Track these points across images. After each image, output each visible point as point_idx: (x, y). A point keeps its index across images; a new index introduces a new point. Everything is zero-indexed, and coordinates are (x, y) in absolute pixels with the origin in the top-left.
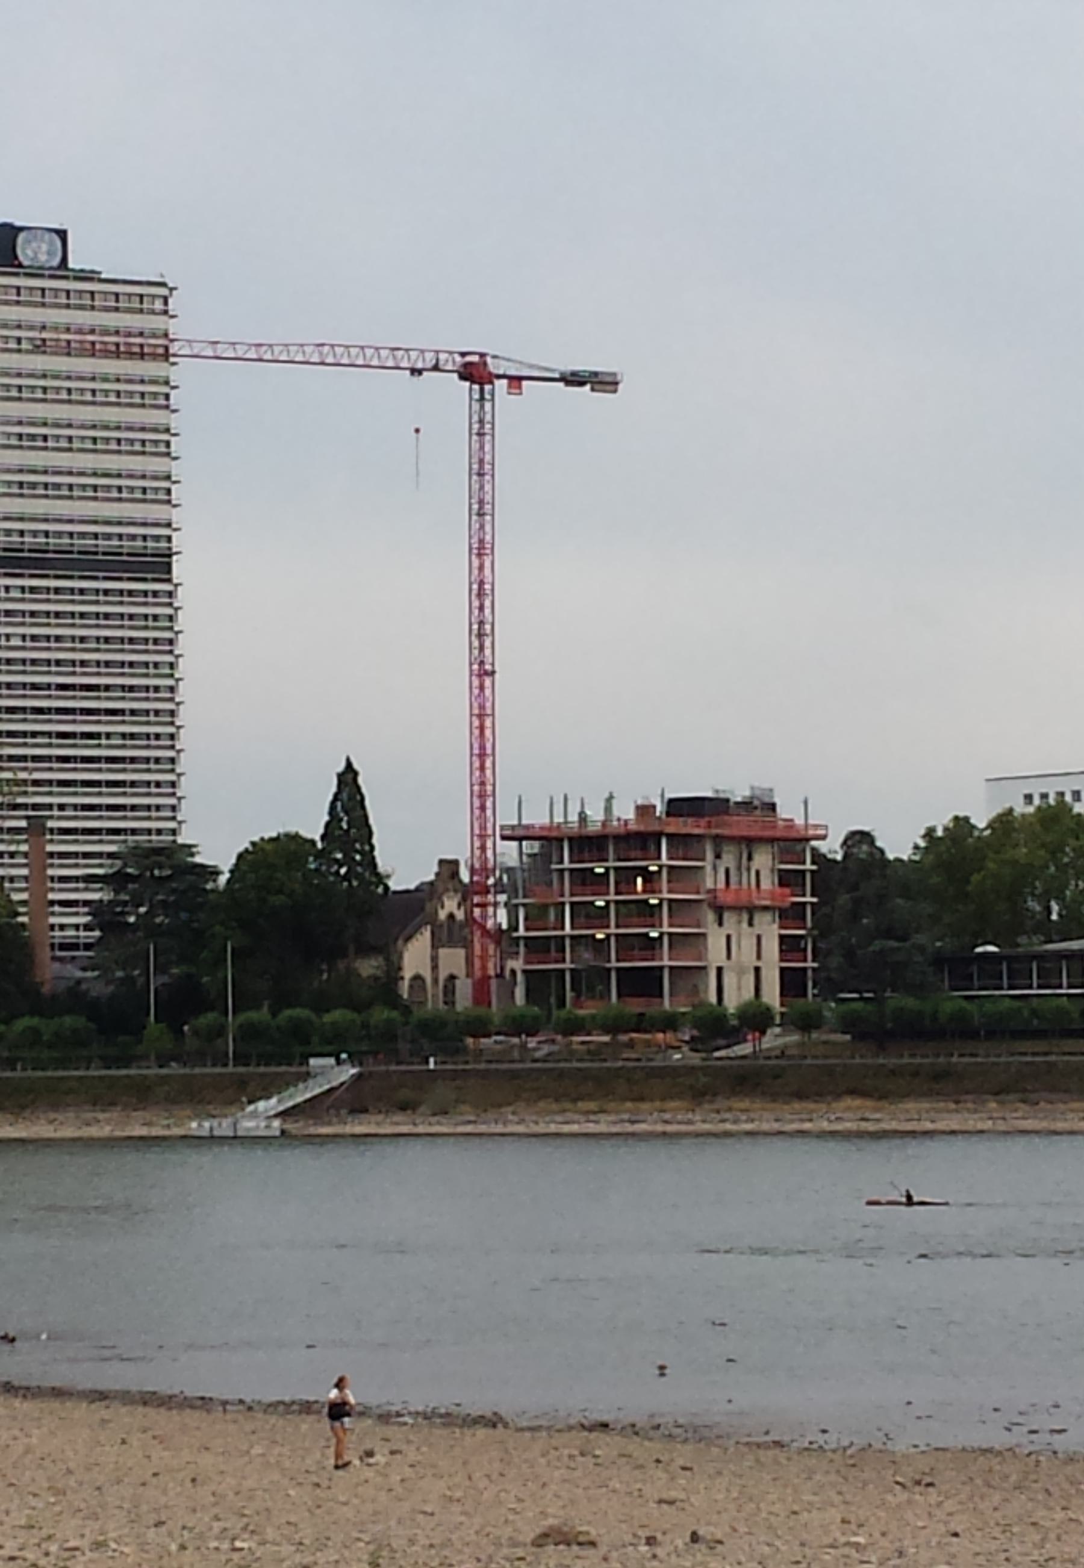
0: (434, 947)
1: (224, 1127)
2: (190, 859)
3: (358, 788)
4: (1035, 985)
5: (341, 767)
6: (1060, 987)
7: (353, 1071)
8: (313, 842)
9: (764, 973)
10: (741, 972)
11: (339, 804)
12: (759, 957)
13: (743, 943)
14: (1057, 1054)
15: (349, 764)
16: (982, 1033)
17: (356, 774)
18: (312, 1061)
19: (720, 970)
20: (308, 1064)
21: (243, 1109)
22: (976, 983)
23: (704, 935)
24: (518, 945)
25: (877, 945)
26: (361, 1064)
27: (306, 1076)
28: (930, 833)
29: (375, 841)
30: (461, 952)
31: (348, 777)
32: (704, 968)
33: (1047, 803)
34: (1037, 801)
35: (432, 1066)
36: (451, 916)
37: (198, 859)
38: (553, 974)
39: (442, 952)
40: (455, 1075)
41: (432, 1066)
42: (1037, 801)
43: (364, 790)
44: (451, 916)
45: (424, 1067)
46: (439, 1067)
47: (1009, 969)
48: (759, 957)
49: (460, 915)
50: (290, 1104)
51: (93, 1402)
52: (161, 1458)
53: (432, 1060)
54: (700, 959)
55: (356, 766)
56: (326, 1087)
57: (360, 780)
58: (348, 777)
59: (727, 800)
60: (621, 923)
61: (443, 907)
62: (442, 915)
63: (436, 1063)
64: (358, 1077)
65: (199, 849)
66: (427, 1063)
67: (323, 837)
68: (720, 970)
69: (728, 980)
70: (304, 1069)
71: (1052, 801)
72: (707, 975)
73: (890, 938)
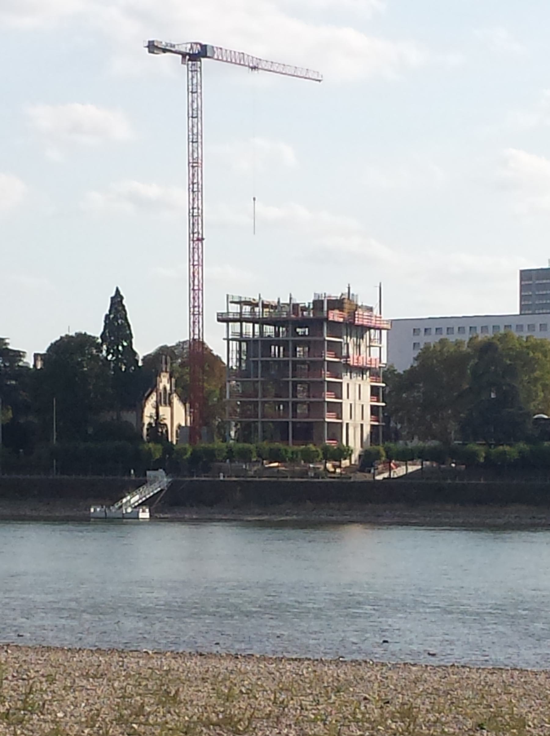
5: (113, 294)
15: (117, 291)
17: (122, 298)
18: (148, 473)
19: (347, 424)
20: (146, 475)
26: (173, 477)
30: (168, 409)
34: (491, 329)
37: (10, 347)
43: (127, 308)
44: (165, 388)
46: (226, 479)
57: (124, 302)
65: (7, 341)
68: (347, 424)
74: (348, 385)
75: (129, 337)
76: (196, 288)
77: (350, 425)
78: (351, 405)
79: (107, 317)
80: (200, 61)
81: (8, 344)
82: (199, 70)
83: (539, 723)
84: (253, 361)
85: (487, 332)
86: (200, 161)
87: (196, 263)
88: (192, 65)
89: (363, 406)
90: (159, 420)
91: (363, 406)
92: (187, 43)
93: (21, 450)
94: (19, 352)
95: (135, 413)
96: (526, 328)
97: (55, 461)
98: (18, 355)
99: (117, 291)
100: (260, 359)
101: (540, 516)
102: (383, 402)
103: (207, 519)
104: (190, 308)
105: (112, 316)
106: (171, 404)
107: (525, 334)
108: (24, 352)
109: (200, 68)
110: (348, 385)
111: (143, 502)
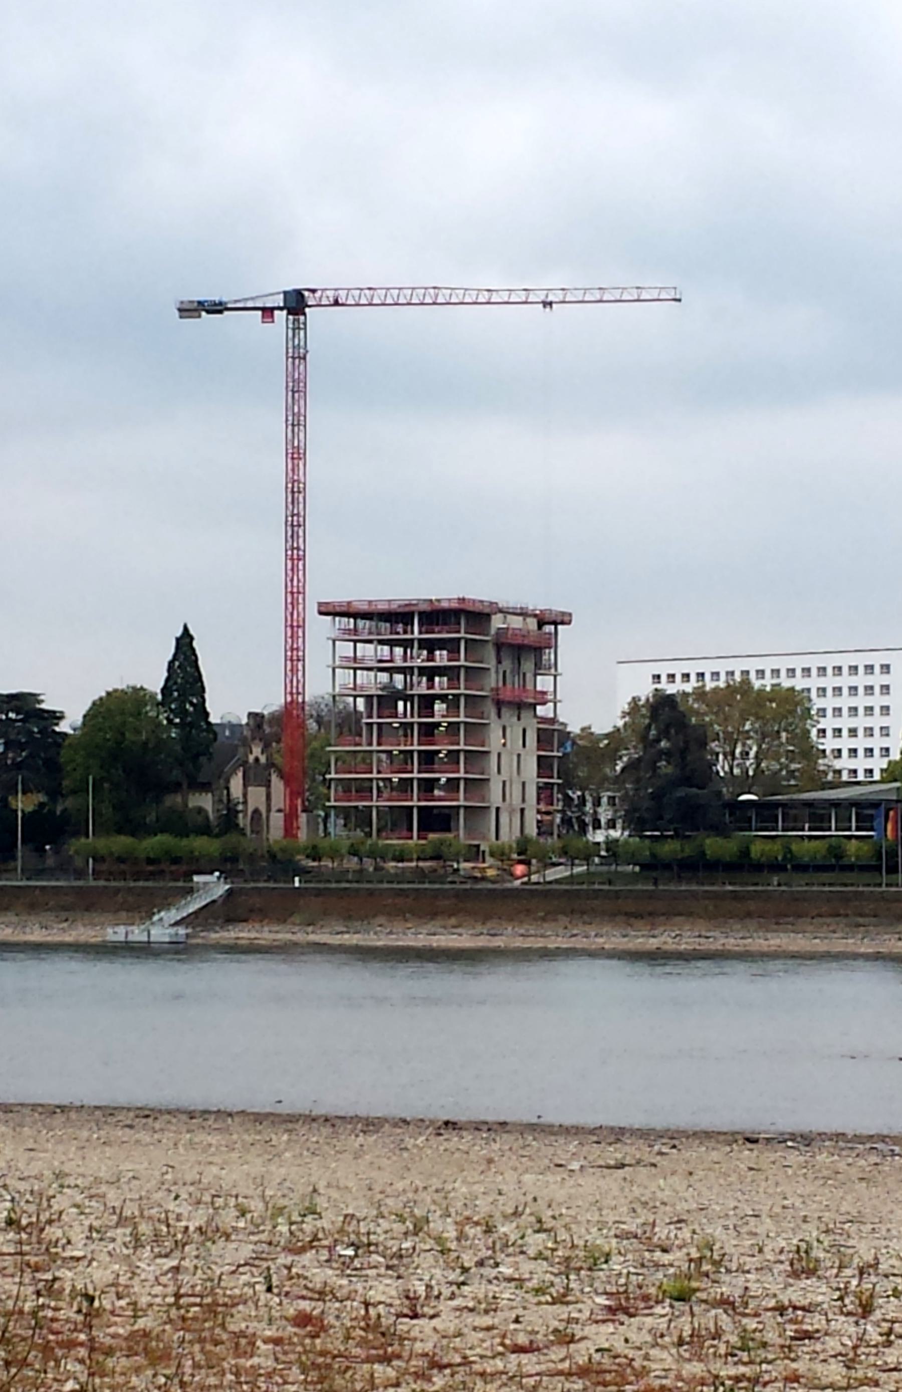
0: (245, 786)
1: (137, 934)
2: (38, 706)
3: (193, 650)
4: (854, 827)
5: (179, 633)
6: (830, 829)
7: (227, 887)
8: (153, 696)
9: (526, 812)
10: (511, 813)
11: (177, 663)
12: (524, 800)
13: (514, 786)
14: (819, 885)
15: (186, 629)
16: (789, 866)
17: (192, 638)
18: (196, 878)
19: (498, 809)
20: (192, 880)
21: (151, 919)
22: (807, 826)
23: (488, 780)
24: (329, 788)
25: (681, 792)
26: (232, 883)
27: (190, 891)
28: (635, 700)
29: (207, 696)
30: (263, 790)
31: (185, 642)
32: (488, 808)
33: (733, 680)
34: (723, 677)
35: (297, 884)
36: (257, 760)
37: (43, 706)
38: (353, 811)
39: (250, 789)
40: (319, 893)
41: (297, 884)
42: (723, 677)
43: (198, 652)
44: (257, 760)
45: (290, 886)
46: (304, 885)
47: (857, 814)
48: (524, 800)
49: (263, 759)
50: (185, 914)
51: (810, 1304)
52: (580, 1311)
53: (297, 879)
54: (483, 801)
55: (192, 632)
56: (208, 900)
57: (195, 644)
58: (185, 642)
59: (101, 699)
60: (469, 768)
61: (251, 752)
62: (251, 758)
63: (300, 881)
64: (230, 892)
65: (42, 697)
66: (293, 882)
67: (163, 690)
68: (498, 809)
69: (504, 819)
70: (190, 885)
71: (738, 677)
72: (490, 813)
73: (691, 786)
74: (499, 755)
75: (201, 691)
76: (295, 624)
77: (501, 811)
78: (504, 783)
79: (171, 664)
80: (304, 314)
81: (42, 701)
82: (302, 326)
83: (338, 1215)
84: (367, 724)
85: (718, 680)
86: (302, 451)
87: (295, 590)
88: (294, 320)
89: (524, 784)
90: (231, 805)
91: (524, 784)
92: (279, 293)
93: (48, 847)
94: (54, 712)
95: (210, 795)
96: (768, 674)
97: (91, 861)
98: (56, 717)
99: (186, 629)
100: (375, 720)
101: (708, 934)
102: (559, 778)
103: (867, 957)
104: (286, 651)
105: (177, 663)
106: (268, 785)
107: (768, 682)
108: (61, 712)
109: (305, 324)
110: (499, 755)
111: (183, 919)
